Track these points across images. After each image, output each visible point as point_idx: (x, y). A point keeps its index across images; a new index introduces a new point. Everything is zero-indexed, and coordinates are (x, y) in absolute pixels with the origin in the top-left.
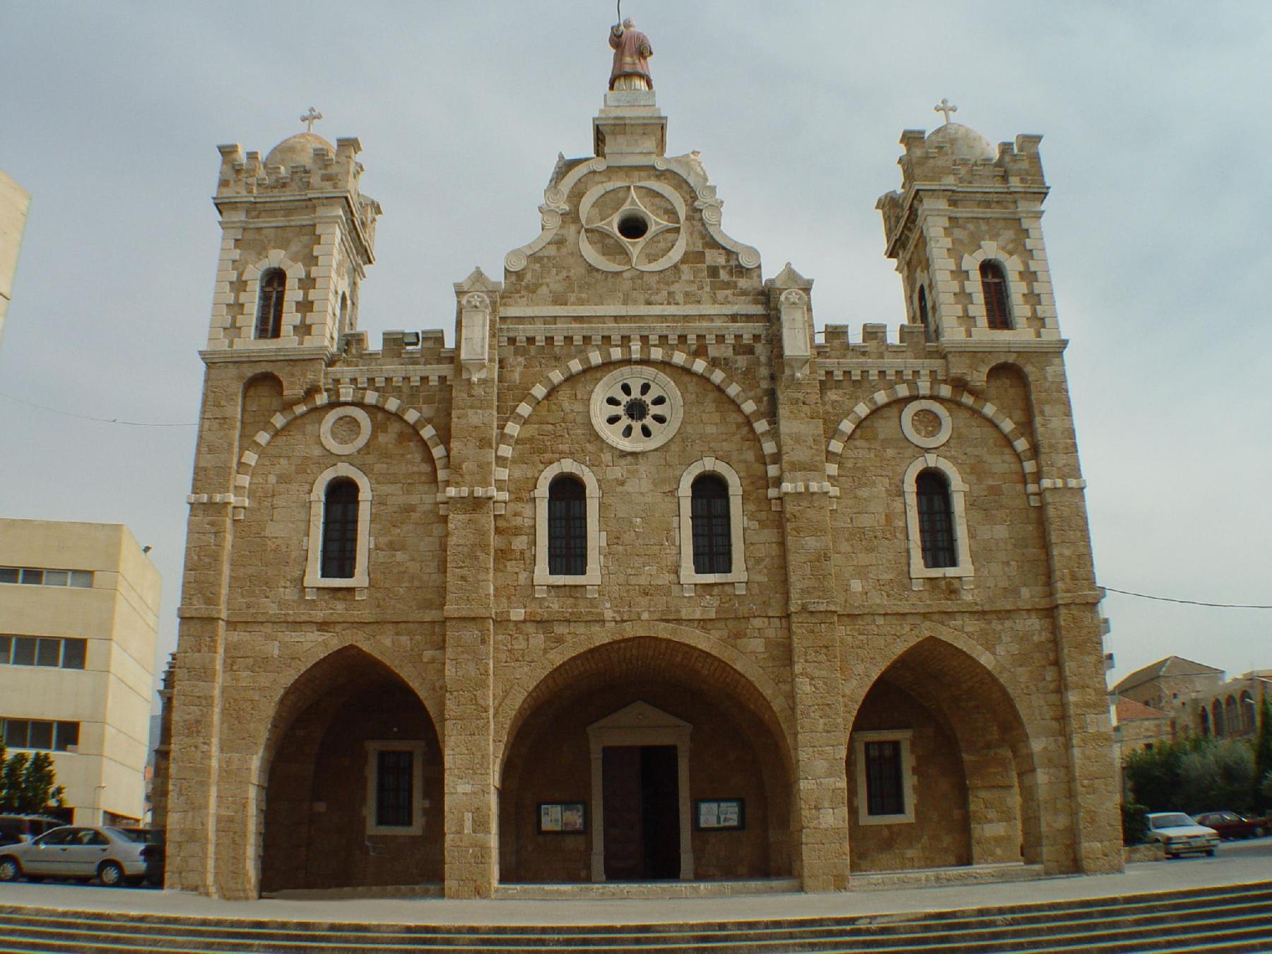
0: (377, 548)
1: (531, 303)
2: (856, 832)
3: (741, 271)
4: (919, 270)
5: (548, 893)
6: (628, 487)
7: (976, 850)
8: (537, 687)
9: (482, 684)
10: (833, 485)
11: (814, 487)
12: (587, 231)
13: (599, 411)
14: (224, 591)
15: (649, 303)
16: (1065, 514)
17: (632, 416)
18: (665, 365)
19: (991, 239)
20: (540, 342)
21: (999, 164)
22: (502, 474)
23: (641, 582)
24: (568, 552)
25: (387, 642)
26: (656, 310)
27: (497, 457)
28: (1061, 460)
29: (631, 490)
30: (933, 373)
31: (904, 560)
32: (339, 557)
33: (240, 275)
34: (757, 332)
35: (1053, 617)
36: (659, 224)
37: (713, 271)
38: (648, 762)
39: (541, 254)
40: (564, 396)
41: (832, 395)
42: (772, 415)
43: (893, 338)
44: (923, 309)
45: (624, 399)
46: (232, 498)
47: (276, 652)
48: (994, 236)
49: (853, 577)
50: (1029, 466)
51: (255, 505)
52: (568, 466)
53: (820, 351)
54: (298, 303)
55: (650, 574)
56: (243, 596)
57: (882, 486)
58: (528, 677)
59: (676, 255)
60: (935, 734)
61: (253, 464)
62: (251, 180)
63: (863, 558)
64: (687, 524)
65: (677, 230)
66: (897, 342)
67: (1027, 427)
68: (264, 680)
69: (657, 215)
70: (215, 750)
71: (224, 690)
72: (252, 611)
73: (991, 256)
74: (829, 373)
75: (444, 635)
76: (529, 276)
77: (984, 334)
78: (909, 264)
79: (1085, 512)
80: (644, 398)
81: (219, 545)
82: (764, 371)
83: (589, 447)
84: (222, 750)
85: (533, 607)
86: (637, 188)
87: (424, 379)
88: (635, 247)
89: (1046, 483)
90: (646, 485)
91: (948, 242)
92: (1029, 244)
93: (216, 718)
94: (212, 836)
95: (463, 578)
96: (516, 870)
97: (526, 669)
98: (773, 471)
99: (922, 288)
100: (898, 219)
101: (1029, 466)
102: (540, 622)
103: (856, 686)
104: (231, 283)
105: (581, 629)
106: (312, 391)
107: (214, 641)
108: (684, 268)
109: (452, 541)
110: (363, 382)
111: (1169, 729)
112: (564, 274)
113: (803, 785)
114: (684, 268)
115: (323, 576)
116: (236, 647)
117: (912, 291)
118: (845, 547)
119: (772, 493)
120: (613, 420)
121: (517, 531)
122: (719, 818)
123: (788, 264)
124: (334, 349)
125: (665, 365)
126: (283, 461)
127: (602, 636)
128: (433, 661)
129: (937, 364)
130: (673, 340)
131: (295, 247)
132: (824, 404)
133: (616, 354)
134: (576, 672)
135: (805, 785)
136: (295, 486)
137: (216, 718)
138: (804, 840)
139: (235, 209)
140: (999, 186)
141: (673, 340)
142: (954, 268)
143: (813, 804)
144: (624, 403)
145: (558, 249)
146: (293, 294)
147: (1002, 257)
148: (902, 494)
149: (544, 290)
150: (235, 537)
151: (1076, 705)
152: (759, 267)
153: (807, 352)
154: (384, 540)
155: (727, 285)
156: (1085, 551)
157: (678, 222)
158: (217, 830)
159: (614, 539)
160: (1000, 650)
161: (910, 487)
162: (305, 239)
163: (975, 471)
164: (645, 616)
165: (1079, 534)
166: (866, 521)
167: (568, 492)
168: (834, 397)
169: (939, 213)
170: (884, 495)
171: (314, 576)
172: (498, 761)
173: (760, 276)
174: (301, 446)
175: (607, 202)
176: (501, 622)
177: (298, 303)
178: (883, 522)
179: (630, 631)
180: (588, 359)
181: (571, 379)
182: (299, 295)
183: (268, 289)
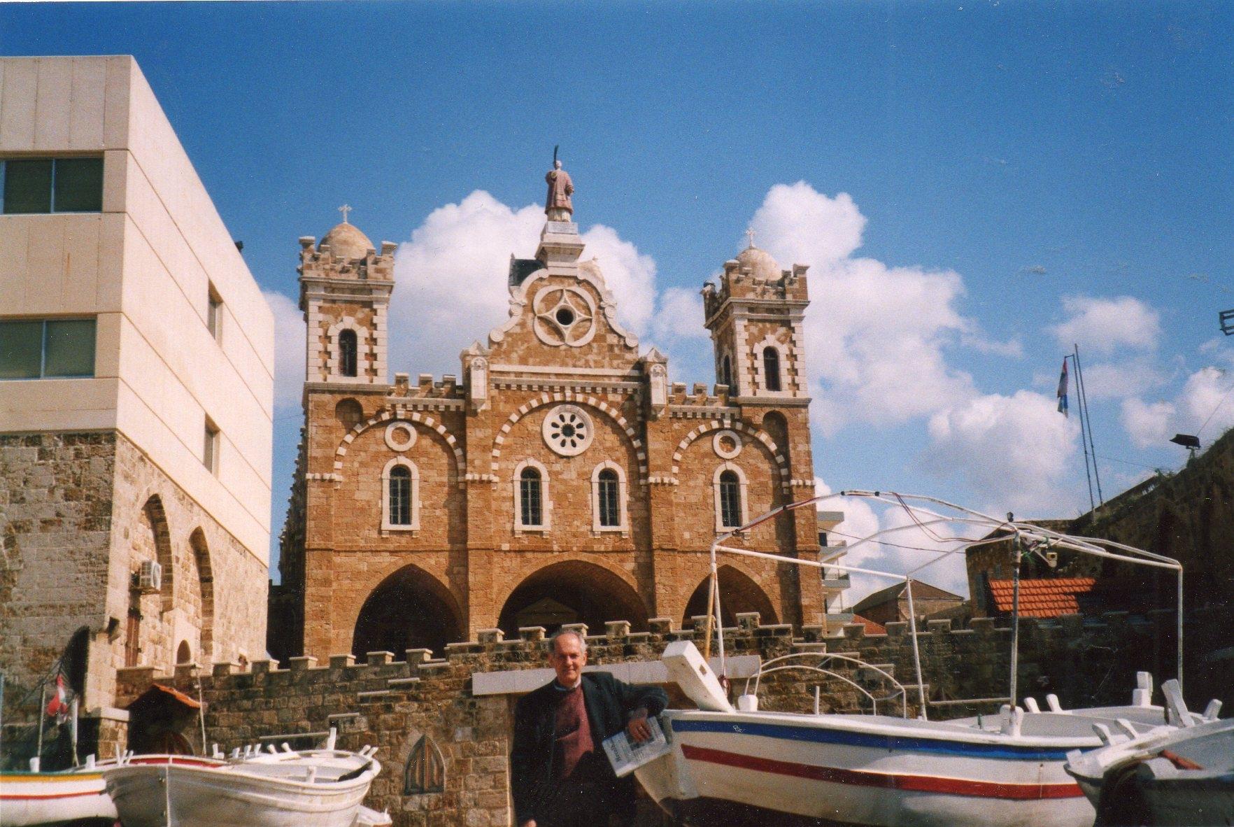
0: (424, 507)
11: (666, 480)
12: (540, 318)
13: (548, 431)
15: (575, 366)
18: (584, 405)
20: (514, 387)
21: (781, 283)
22: (495, 466)
23: (575, 529)
24: (532, 511)
25: (433, 562)
28: (803, 469)
30: (732, 415)
32: (402, 512)
37: (611, 347)
40: (527, 420)
41: (676, 426)
42: (642, 436)
43: (710, 393)
46: (336, 477)
48: (774, 332)
52: (532, 463)
57: (701, 479)
63: (690, 520)
73: (771, 344)
74: (675, 413)
76: (505, 346)
77: (764, 393)
78: (719, 337)
83: (543, 452)
87: (447, 407)
88: (567, 330)
89: (794, 482)
90: (574, 475)
91: (745, 335)
92: (794, 337)
98: (643, 469)
105: (539, 555)
106: (382, 410)
108: (595, 345)
109: (470, 505)
110: (410, 407)
114: (595, 345)
119: (642, 482)
120: (555, 436)
125: (584, 405)
126: (363, 454)
127: (551, 560)
128: (459, 573)
129: (735, 410)
130: (588, 390)
131: (360, 315)
133: (558, 397)
136: (371, 470)
140: (780, 301)
141: (588, 390)
146: (362, 349)
147: (777, 345)
148: (712, 484)
149: (514, 355)
154: (427, 503)
155: (618, 357)
160: (763, 574)
161: (717, 480)
162: (367, 310)
163: (754, 473)
169: (742, 317)
175: (550, 300)
179: (566, 557)
181: (532, 411)
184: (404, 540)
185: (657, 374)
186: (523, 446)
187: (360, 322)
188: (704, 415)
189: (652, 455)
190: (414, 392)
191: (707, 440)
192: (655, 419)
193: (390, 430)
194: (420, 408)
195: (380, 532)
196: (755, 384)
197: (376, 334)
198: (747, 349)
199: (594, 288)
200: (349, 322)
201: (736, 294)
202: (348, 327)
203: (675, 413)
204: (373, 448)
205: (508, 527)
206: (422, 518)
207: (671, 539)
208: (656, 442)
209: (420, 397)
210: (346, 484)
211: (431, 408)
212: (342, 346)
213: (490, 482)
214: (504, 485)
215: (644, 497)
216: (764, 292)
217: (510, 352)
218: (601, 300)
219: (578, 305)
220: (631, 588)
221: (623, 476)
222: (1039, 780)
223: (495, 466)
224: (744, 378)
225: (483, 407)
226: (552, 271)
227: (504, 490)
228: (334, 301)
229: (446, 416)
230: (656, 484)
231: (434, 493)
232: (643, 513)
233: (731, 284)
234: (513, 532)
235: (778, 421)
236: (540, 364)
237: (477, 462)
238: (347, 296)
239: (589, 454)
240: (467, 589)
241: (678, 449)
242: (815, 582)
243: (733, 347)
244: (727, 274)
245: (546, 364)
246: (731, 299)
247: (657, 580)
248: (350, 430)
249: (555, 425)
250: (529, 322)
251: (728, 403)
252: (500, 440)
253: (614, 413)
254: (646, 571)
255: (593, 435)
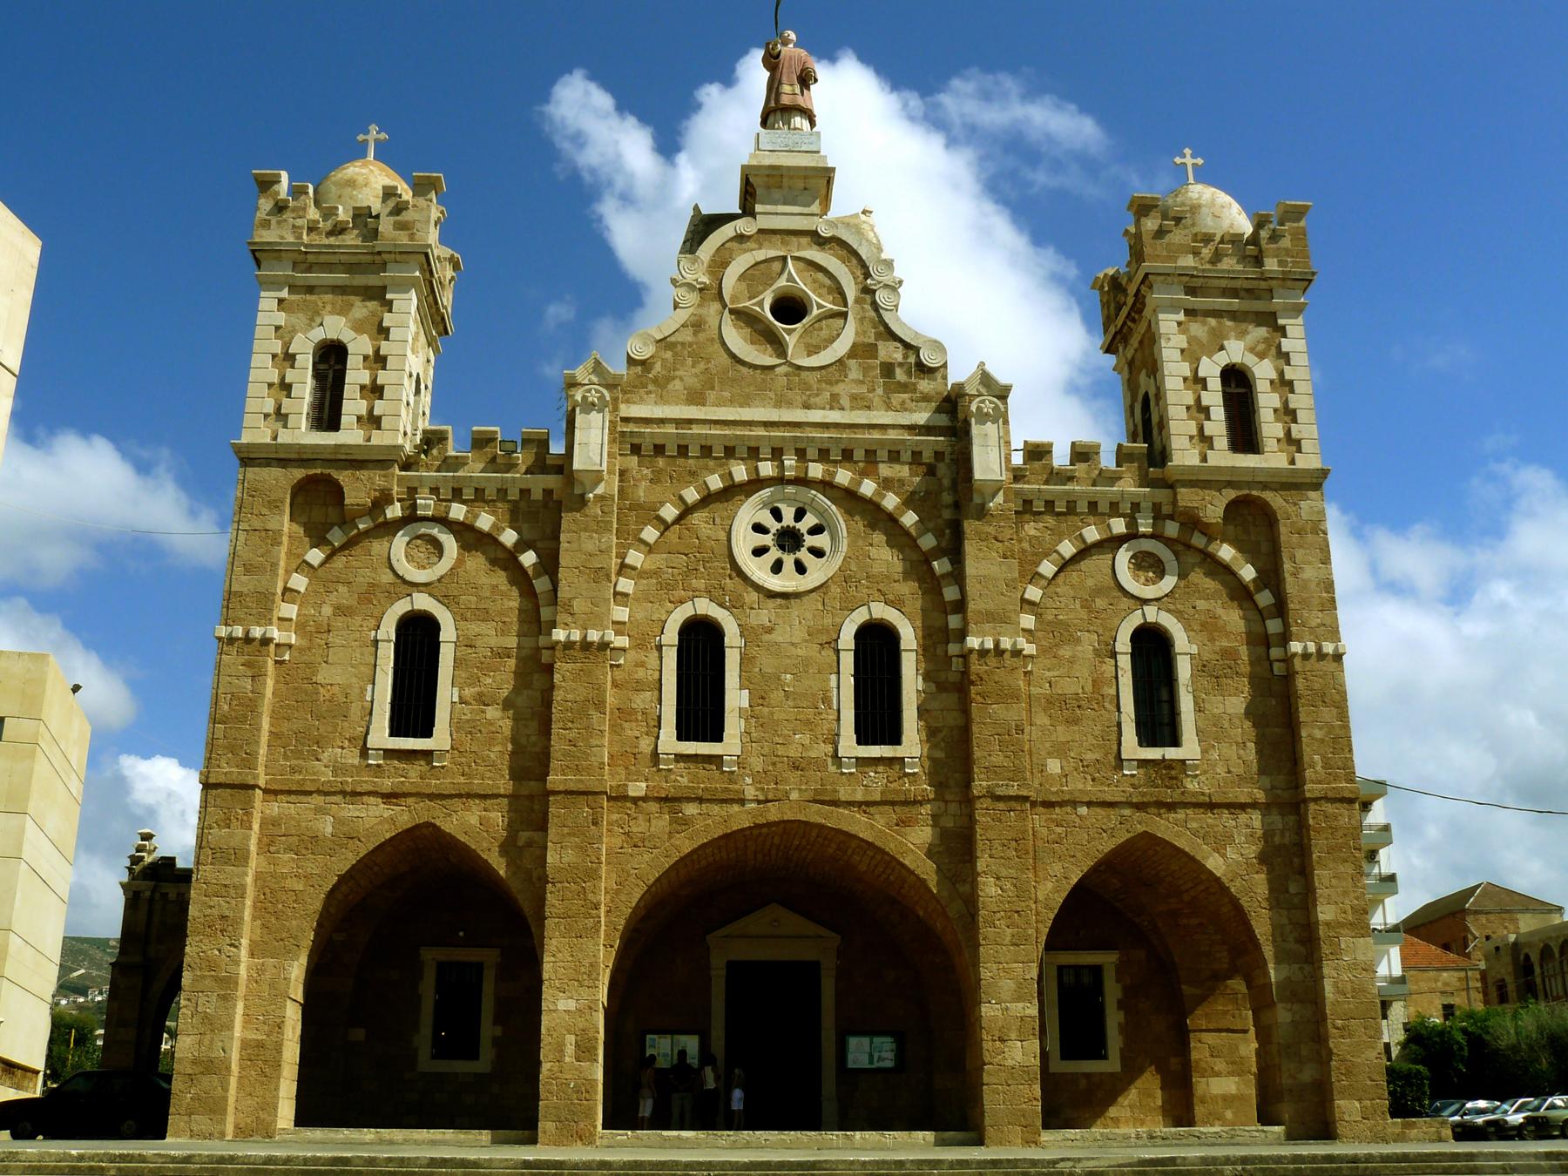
1: (662, 400)
2: (1050, 1082)
3: (923, 370)
4: (1144, 372)
5: (665, 1139)
6: (776, 636)
7: (1199, 1111)
8: (658, 880)
9: (593, 875)
10: (1029, 642)
11: (1006, 643)
12: (732, 312)
13: (743, 542)
14: (263, 751)
15: (807, 407)
16: (1317, 686)
17: (782, 548)
18: (826, 486)
19: (1237, 338)
20: (671, 450)
22: (621, 613)
23: (793, 750)
24: (701, 713)
26: (816, 416)
27: (616, 594)
28: (1315, 618)
29: (780, 639)
31: (1114, 737)
32: (413, 710)
33: (287, 345)
34: (939, 448)
35: (1298, 814)
36: (820, 306)
37: (888, 369)
38: (793, 973)
39: (672, 339)
40: (697, 518)
41: (1031, 529)
42: (955, 552)
43: (1107, 461)
44: (1147, 422)
45: (774, 526)
46: (275, 634)
47: (329, 829)
48: (1241, 335)
49: (1050, 754)
50: (1274, 626)
51: (304, 643)
52: (705, 607)
53: (1018, 474)
54: (363, 387)
55: (800, 743)
56: (286, 757)
57: (1088, 643)
58: (649, 866)
59: (841, 347)
60: (1152, 959)
61: (302, 590)
62: (299, 222)
63: (1062, 733)
64: (848, 682)
65: (844, 315)
66: (1113, 466)
67: (1271, 576)
68: (312, 866)
69: (820, 296)
70: (244, 953)
71: (258, 876)
72: (298, 777)
73: (1237, 359)
74: (1028, 503)
75: (546, 813)
76: (658, 367)
77: (1223, 457)
78: (1131, 364)
79: (1343, 685)
80: (798, 525)
81: (259, 694)
82: (947, 498)
84: (252, 955)
85: (658, 781)
86: (795, 258)
88: (792, 336)
90: (799, 634)
91: (1181, 341)
93: (247, 914)
94: (235, 1067)
95: (571, 742)
96: (620, 1115)
97: (647, 857)
98: (954, 621)
99: (1146, 395)
100: (1119, 308)
101: (1274, 626)
102: (666, 799)
103: (1052, 887)
104: (274, 356)
105: (716, 809)
106: (384, 499)
107: (248, 814)
108: (852, 363)
109: (558, 695)
110: (445, 493)
111: (1479, 985)
112: (702, 366)
113: (985, 1010)
115: (391, 735)
116: (275, 822)
117: (1134, 400)
118: (1042, 719)
119: (953, 649)
120: (759, 552)
121: (639, 687)
122: (871, 1056)
123: (983, 364)
124: (408, 448)
125: (826, 486)
126: (342, 589)
127: (741, 818)
128: (529, 844)
129: (1162, 495)
132: (1020, 541)
133: (767, 469)
134: (704, 863)
135: (988, 1011)
137: (247, 914)
138: (987, 1059)
139: (279, 259)
141: (835, 455)
142: (1188, 373)
143: (997, 1034)
144: (773, 531)
145: (695, 334)
146: (357, 375)
147: (1250, 360)
148: (1114, 655)
149: (677, 385)
150: (277, 682)
151: (1328, 924)
152: (945, 366)
153: (1005, 476)
154: (469, 692)
155: (904, 387)
156: (1342, 733)
157: (846, 305)
158: (241, 1059)
159: (758, 699)
161: (1124, 644)
163: (1206, 628)
164: (794, 796)
165: (1335, 711)
166: (1069, 687)
167: (701, 644)
168: (1033, 532)
169: (1172, 307)
170: (1090, 655)
171: (381, 736)
172: (608, 971)
173: (945, 378)
174: (361, 567)
175: (756, 277)
176: (620, 798)
177: (363, 387)
178: (1089, 688)
179: (773, 813)
180: (730, 474)
181: (708, 499)
182: (365, 377)
183: (322, 367)
184: (414, 771)
185: (984, 418)
186: (691, 571)
187: (358, 328)
188: (1093, 506)
189: (972, 588)
190: (458, 463)
191: (1099, 562)
192: (982, 513)
193: (400, 541)
194: (468, 494)
195: (364, 752)
196: (1205, 440)
197: (385, 348)
198: (1186, 369)
199: (855, 253)
200: (335, 327)
201: (1157, 257)
202: (332, 335)
203: (1028, 503)
204: (363, 577)
205: (645, 745)
206: (456, 725)
207: (1017, 774)
208: (983, 563)
209: (474, 470)
210: (301, 650)
211: (491, 493)
212: (318, 375)
213: (604, 646)
214: (641, 656)
215: (954, 683)
216: (1217, 257)
217: (669, 379)
218: (867, 275)
219: (817, 286)
220: (923, 882)
221: (909, 637)
222: (1302, 602)
223: (621, 613)
224: (1180, 430)
225: (600, 490)
226: (764, 222)
227: (642, 665)
228: (310, 289)
229: (521, 511)
230: (983, 653)
231: (485, 668)
232: (953, 719)
233: (1146, 239)
234: (655, 754)
235: (1254, 517)
236: (731, 402)
237: (578, 606)
238: (340, 277)
239: (835, 590)
240: (544, 880)
241: (1035, 577)
242: (1348, 869)
243: (1153, 367)
244: (1138, 222)
245: (746, 402)
246: (1147, 265)
247: (981, 865)
248: (319, 540)
249: (759, 528)
250: (713, 322)
251: (1144, 481)
252: (635, 558)
253: (891, 502)
254: (958, 848)
255: (844, 546)
